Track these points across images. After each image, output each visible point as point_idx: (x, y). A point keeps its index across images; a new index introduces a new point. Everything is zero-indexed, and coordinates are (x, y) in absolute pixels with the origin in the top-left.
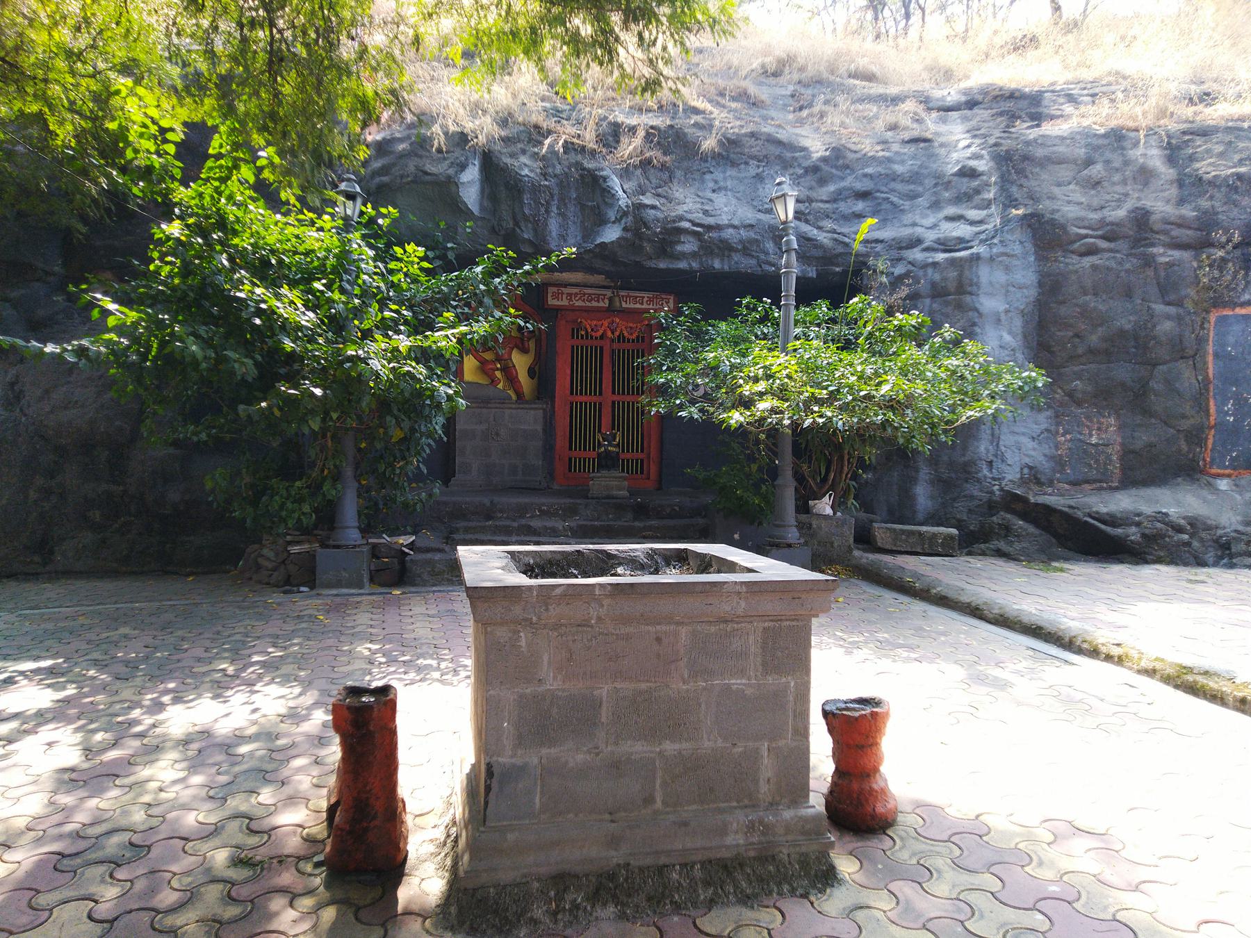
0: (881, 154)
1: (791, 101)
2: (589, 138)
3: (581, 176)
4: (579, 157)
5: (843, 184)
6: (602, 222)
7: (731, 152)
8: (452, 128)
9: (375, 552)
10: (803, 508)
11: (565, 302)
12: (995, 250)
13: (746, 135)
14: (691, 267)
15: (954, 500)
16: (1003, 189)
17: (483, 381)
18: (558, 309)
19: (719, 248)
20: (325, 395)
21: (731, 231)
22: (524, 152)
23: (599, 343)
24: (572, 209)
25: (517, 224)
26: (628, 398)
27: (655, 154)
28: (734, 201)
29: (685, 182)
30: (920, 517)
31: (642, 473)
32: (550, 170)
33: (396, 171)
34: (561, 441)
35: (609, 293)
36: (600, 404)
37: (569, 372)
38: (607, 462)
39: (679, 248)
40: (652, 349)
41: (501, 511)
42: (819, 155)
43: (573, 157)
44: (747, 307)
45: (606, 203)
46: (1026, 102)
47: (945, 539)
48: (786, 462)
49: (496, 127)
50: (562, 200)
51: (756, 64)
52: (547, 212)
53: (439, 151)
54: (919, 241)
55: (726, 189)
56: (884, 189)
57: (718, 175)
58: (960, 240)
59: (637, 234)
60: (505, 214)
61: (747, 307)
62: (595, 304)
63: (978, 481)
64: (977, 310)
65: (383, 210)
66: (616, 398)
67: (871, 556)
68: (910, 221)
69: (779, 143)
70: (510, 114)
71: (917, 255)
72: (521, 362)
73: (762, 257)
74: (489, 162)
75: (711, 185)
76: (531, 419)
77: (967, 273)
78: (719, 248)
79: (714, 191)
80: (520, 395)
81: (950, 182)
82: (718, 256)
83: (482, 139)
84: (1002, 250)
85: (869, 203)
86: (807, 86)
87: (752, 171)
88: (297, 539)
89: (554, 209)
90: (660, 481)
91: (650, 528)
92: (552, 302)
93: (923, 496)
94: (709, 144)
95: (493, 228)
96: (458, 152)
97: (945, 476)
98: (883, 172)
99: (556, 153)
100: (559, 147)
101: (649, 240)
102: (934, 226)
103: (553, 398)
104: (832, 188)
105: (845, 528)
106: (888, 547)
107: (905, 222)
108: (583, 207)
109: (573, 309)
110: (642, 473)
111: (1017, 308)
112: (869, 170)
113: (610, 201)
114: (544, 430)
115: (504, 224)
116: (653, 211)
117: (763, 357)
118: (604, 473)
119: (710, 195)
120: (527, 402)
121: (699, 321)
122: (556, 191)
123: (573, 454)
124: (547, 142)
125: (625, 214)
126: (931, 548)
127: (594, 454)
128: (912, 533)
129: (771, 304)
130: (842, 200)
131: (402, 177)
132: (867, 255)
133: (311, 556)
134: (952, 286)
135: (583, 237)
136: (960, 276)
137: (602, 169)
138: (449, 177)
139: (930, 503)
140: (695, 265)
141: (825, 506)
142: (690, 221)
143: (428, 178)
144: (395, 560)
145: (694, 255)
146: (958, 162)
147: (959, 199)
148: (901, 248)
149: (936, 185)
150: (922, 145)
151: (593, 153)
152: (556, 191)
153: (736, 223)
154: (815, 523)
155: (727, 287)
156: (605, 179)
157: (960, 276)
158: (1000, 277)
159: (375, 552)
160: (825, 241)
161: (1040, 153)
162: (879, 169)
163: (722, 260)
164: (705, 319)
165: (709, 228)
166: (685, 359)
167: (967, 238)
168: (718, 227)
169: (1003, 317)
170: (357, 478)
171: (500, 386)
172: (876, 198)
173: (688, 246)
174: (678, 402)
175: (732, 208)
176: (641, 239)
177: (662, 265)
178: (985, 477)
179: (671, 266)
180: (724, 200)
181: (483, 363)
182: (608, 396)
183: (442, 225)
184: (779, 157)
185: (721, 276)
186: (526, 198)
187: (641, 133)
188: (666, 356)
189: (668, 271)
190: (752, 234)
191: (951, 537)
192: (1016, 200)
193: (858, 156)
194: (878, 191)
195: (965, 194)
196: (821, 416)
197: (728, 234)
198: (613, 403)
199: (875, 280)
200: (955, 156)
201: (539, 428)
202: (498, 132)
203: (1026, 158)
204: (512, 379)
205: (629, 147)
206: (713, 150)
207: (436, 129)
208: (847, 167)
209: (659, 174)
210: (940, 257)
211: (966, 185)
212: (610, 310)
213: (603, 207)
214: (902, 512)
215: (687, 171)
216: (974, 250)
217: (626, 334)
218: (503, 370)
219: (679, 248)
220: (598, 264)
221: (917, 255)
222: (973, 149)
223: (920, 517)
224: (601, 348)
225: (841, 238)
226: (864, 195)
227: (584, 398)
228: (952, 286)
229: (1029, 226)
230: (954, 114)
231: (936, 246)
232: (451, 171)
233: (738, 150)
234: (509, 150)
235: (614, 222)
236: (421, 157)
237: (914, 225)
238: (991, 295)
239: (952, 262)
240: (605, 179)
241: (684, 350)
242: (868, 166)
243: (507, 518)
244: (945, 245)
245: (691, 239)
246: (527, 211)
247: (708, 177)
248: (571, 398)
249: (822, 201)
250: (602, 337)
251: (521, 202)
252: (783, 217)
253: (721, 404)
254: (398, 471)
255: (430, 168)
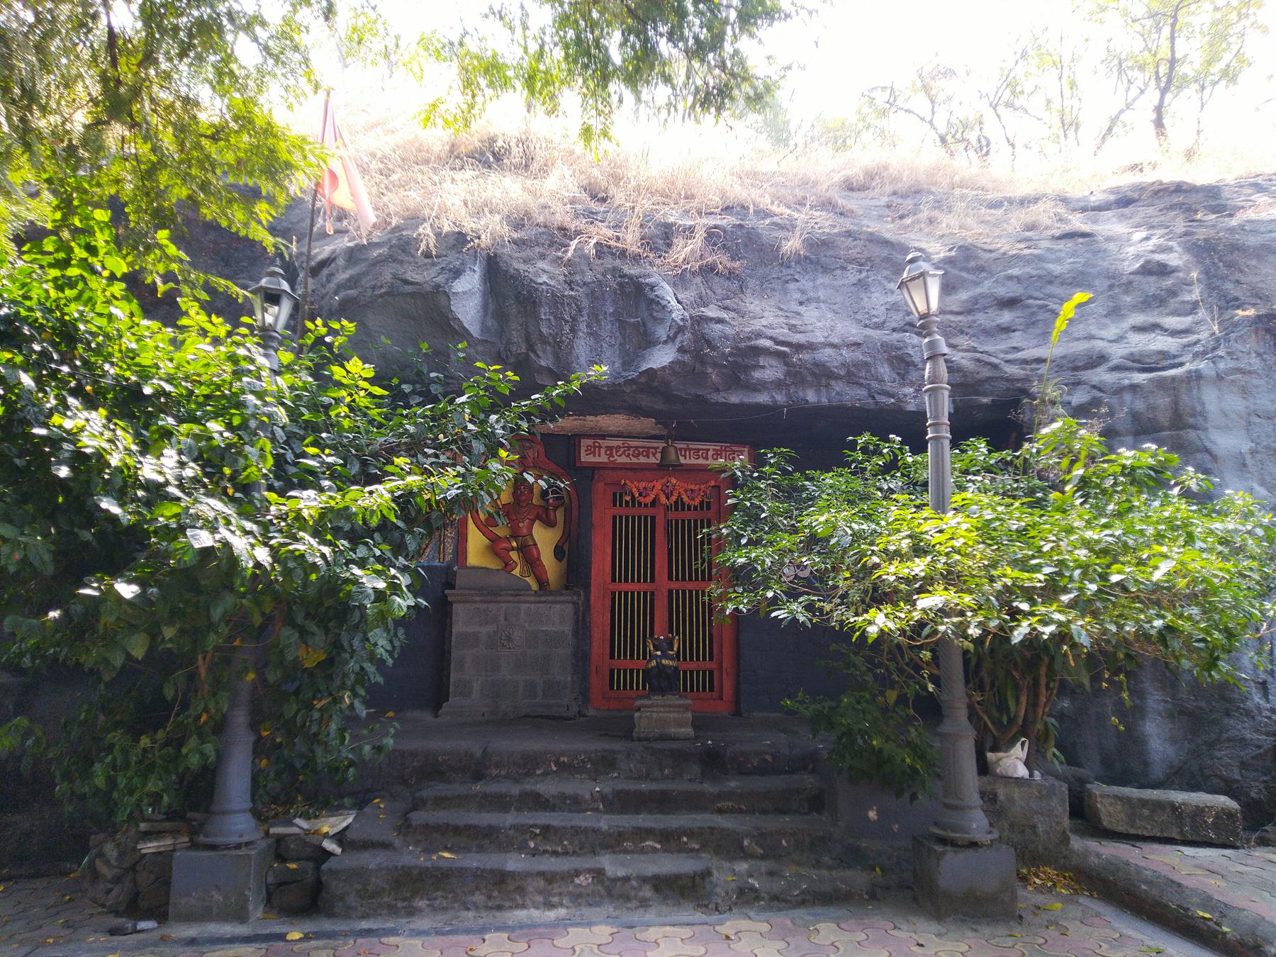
0: (1027, 252)
1: (887, 212)
2: (631, 239)
3: (620, 284)
4: (618, 262)
5: (979, 290)
6: (648, 342)
7: (820, 256)
8: (447, 228)
9: (279, 850)
10: (984, 768)
11: (603, 458)
12: (1222, 366)
13: (839, 235)
14: (775, 401)
15: (1211, 745)
16: (1210, 287)
17: (493, 564)
18: (595, 468)
19: (813, 374)
20: (142, 596)
21: (829, 351)
22: (543, 257)
23: (650, 512)
24: (607, 328)
25: (531, 347)
26: (690, 586)
27: (721, 260)
28: (830, 315)
29: (762, 292)
30: (1158, 771)
31: (711, 689)
32: (578, 278)
33: (367, 282)
34: (241, 930)
35: (661, 445)
36: (652, 594)
37: (609, 550)
38: (661, 682)
39: (757, 374)
40: (724, 514)
41: (497, 766)
42: (942, 255)
43: (609, 262)
44: (864, 450)
45: (655, 319)
46: (1200, 195)
47: (1217, 817)
48: (958, 697)
49: (507, 228)
50: (595, 316)
51: (837, 178)
52: (573, 330)
53: (427, 255)
54: (1101, 359)
55: (817, 300)
56: (1037, 294)
57: (806, 283)
58: (1164, 354)
59: (701, 359)
60: (516, 335)
61: (864, 450)
62: (643, 460)
63: (1248, 714)
64: (1208, 451)
65: (336, 326)
66: (674, 585)
67: (1092, 844)
68: (1083, 333)
69: (886, 243)
70: (527, 214)
71: (1101, 375)
72: (544, 539)
73: (874, 384)
74: (494, 269)
75: (798, 296)
76: (556, 618)
77: (1184, 398)
78: (813, 374)
79: (801, 303)
80: (543, 583)
81: (1130, 283)
82: (811, 386)
83: (485, 240)
84: (1232, 364)
85: (1019, 313)
86: (905, 196)
87: (852, 276)
88: (159, 827)
89: (583, 327)
90: (737, 702)
91: (730, 795)
92: (585, 458)
93: (1159, 740)
94: (792, 245)
95: (499, 353)
96: (452, 256)
97: (1190, 706)
98: (1034, 272)
99: (586, 257)
100: (590, 249)
101: (716, 365)
102: (1119, 339)
103: (587, 588)
104: (964, 295)
105: (1055, 801)
106: (1121, 828)
107: (1076, 335)
108: (622, 325)
109: (616, 468)
110: (711, 689)
111: (1267, 447)
112: (1015, 272)
113: (659, 315)
114: (576, 633)
115: (514, 349)
116: (719, 326)
117: (901, 519)
118: (657, 699)
119: (794, 307)
120: (551, 593)
121: (790, 473)
122: (585, 303)
123: (616, 663)
124: (574, 244)
125: (681, 330)
126: (1194, 830)
127: (641, 664)
128: (1158, 805)
129: (901, 443)
130: (979, 310)
131: (374, 288)
132: (1027, 379)
133: (164, 858)
134: (1164, 418)
135: (623, 364)
136: (1176, 403)
137: (649, 276)
138: (438, 286)
139: (1171, 751)
140: (780, 398)
141: (1014, 762)
142: (771, 338)
143: (409, 288)
144: (311, 865)
145: (779, 384)
146: (1138, 257)
147: (1146, 304)
148: (1076, 369)
149: (1111, 287)
150: (1081, 240)
151: (636, 258)
152: (585, 303)
153: (836, 340)
154: (1002, 793)
155: (832, 428)
156: (652, 287)
157: (1176, 403)
158: (1235, 403)
159: (279, 850)
160: (964, 361)
161: (1252, 241)
162: (1028, 270)
163: (818, 391)
164: (800, 468)
165: (799, 347)
166: (774, 528)
167: (1173, 351)
168: (811, 347)
169: (1249, 461)
170: (254, 726)
171: (517, 572)
172: (1028, 306)
173: (770, 371)
174: (770, 594)
175: (828, 323)
176: (703, 363)
177: (734, 399)
178: (1258, 708)
179: (746, 400)
180: (816, 313)
181: (494, 539)
182: (663, 584)
183: (424, 347)
184: (888, 259)
185: (818, 412)
186: (544, 312)
187: (700, 235)
188: (746, 524)
189: (741, 406)
190: (858, 355)
191: (1230, 815)
192: (1236, 299)
193: (993, 255)
194: (1031, 297)
195: (1155, 297)
196: (1045, 623)
197: (825, 355)
198: (670, 592)
199: (1043, 412)
200: (1131, 250)
201: (568, 629)
202: (506, 231)
203: (1234, 248)
204: (532, 562)
205: (683, 250)
206: (797, 254)
207: (426, 230)
208: (981, 269)
209: (727, 283)
210: (1140, 378)
211: (1152, 285)
212: (665, 467)
213: (649, 324)
214: (1125, 765)
215: (764, 280)
216: (1187, 367)
217: (685, 499)
218: (520, 549)
219: (757, 374)
220: (645, 401)
221: (1101, 375)
222: (1154, 241)
223: (1158, 771)
224: (653, 518)
225: (985, 358)
226: (1010, 303)
227: (630, 587)
228: (1164, 418)
229: (1268, 331)
230: (1109, 214)
231: (1130, 364)
232: (440, 279)
233: (831, 253)
234: (523, 254)
235: (665, 342)
236: (401, 262)
237: (1091, 337)
238: (1226, 429)
239: (1161, 384)
240: (652, 287)
241: (773, 513)
242: (1010, 268)
243: (507, 777)
244: (1141, 363)
245: (774, 363)
246: (545, 330)
247: (792, 286)
248: (612, 587)
249: (952, 313)
250: (654, 503)
251: (537, 318)
252: (922, 308)
253: (843, 597)
254: (316, 715)
255: (411, 275)
